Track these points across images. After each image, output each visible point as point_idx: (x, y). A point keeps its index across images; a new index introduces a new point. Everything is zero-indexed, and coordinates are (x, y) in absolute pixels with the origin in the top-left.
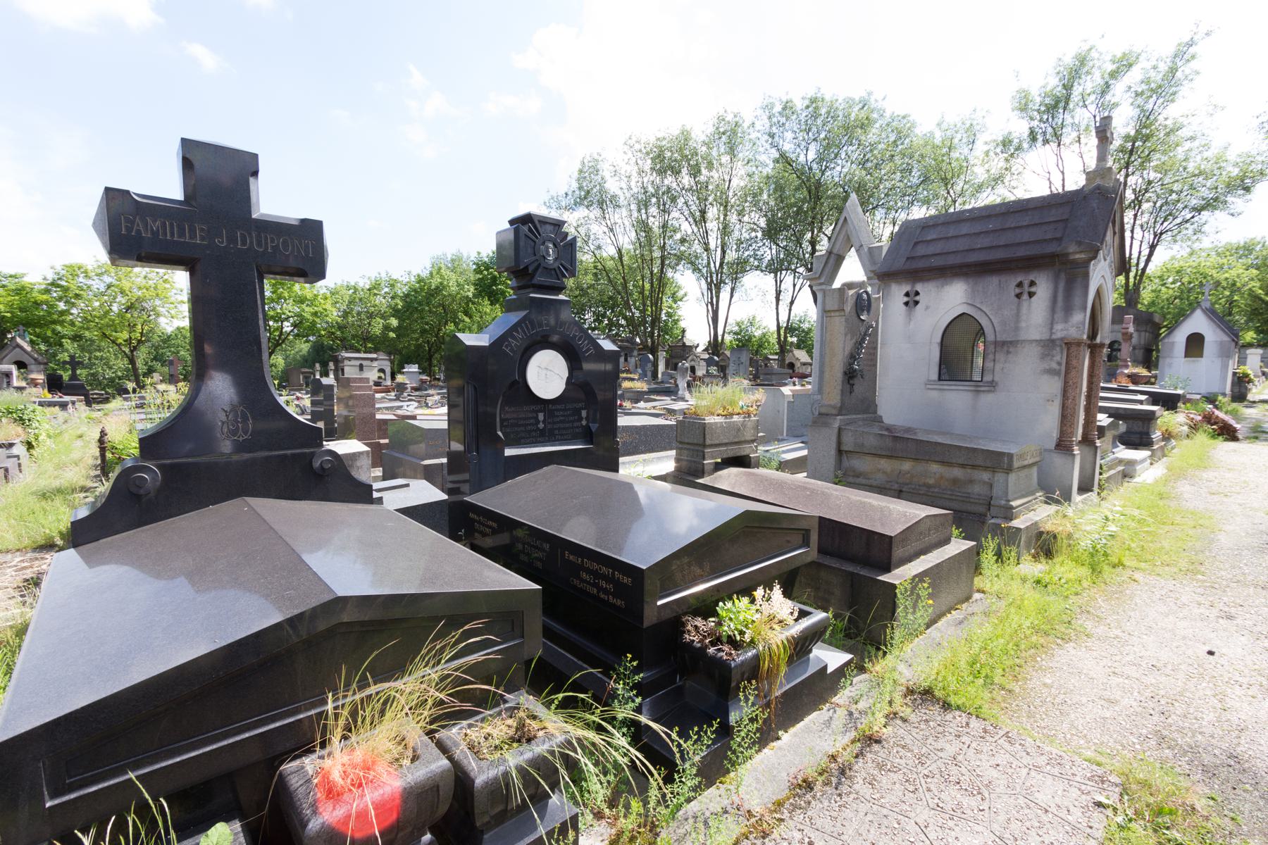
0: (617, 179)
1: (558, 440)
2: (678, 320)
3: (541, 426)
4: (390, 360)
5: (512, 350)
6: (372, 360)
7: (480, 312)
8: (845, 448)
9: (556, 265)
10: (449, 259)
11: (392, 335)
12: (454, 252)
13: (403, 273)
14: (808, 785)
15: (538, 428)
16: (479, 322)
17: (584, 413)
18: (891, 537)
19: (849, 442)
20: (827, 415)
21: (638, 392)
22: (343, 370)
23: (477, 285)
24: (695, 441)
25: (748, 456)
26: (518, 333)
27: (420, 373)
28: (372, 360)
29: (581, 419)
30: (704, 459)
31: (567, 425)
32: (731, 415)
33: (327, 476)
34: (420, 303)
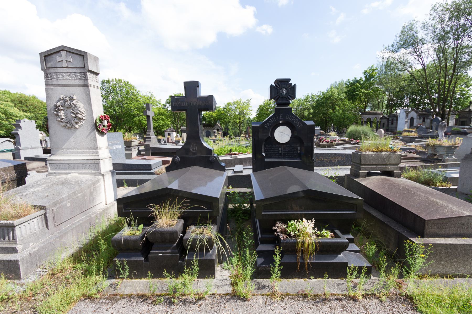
0: (425, 29)
1: (287, 157)
2: (468, 97)
3: (280, 152)
7: (344, 104)
10: (338, 84)
11: (311, 116)
12: (340, 80)
13: (318, 92)
14: (305, 296)
16: (343, 108)
18: (425, 220)
21: (411, 137)
23: (346, 93)
24: (357, 162)
25: (392, 171)
26: (270, 121)
27: (320, 130)
29: (298, 150)
30: (360, 170)
31: (291, 152)
32: (382, 151)
34: (322, 103)
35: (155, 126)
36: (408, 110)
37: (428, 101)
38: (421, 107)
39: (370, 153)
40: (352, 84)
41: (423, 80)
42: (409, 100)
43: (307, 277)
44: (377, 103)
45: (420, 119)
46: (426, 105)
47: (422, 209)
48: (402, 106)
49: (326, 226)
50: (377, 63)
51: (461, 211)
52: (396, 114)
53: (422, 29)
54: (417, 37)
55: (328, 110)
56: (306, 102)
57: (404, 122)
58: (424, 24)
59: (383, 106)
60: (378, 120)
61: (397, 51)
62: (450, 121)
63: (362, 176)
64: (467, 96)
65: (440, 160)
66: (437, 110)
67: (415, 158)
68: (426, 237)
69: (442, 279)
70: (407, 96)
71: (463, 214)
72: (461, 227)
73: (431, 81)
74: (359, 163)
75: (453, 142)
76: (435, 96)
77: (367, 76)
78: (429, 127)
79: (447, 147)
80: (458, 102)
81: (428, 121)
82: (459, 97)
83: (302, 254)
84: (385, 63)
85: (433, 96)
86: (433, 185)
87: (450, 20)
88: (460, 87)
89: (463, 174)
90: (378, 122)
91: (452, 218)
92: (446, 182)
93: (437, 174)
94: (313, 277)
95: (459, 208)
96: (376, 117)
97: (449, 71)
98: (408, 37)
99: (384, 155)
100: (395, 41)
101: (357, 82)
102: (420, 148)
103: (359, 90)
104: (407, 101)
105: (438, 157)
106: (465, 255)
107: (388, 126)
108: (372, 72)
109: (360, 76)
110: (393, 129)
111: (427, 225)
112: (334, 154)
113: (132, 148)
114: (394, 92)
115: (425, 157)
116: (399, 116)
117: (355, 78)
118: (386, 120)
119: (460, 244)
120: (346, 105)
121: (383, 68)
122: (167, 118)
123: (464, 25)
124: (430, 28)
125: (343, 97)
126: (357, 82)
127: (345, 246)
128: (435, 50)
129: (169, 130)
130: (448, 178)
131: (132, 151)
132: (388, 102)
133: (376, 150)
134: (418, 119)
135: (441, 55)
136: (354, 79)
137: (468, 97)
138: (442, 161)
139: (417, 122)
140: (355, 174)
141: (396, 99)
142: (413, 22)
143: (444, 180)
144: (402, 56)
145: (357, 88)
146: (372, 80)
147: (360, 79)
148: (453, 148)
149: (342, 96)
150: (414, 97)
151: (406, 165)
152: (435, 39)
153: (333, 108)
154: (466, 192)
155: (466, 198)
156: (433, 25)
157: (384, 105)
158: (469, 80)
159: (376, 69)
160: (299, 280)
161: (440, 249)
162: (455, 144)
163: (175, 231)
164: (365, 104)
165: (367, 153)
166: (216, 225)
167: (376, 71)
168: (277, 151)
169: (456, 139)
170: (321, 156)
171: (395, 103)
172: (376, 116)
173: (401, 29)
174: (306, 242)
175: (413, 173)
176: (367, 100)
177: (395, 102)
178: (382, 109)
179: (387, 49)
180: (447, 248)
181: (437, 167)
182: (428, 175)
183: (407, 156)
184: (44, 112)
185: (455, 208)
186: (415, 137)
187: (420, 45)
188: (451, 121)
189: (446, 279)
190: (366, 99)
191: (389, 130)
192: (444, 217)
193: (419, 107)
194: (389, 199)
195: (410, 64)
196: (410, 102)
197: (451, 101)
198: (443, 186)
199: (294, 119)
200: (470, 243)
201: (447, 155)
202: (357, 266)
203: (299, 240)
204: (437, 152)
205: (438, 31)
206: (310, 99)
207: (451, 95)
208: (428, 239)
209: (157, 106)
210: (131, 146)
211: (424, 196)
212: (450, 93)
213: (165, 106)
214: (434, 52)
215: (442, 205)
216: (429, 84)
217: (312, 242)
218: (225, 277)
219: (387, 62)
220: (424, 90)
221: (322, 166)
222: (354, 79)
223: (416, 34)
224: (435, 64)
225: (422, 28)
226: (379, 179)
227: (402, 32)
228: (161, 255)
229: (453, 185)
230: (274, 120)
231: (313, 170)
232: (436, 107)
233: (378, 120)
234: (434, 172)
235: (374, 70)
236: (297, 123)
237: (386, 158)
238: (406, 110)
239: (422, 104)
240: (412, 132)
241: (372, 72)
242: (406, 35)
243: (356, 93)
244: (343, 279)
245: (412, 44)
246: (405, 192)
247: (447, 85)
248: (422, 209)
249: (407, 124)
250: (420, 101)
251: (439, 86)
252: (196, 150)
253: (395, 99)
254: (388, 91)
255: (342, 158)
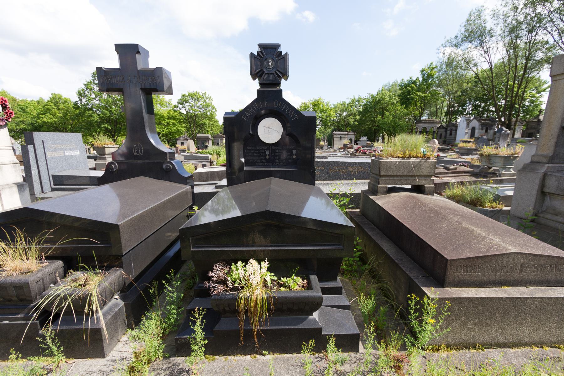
0: (495, 18)
2: (539, 105)
3: (267, 157)
4: (355, 135)
5: (247, 118)
6: (345, 135)
8: (547, 190)
9: (273, 71)
10: (391, 85)
11: (357, 123)
12: (393, 81)
15: (266, 158)
17: (294, 152)
18: (447, 260)
19: (552, 185)
20: (538, 163)
21: (468, 149)
22: (334, 139)
27: (367, 140)
28: (345, 135)
30: (379, 184)
32: (410, 157)
33: (169, 171)
35: (164, 133)
36: (469, 118)
37: (494, 109)
38: (485, 115)
39: (394, 159)
40: (406, 86)
41: (489, 83)
42: (472, 107)
43: (257, 351)
44: (435, 110)
45: (482, 129)
46: (491, 113)
47: (449, 241)
48: (463, 114)
49: (297, 269)
50: (437, 59)
51: (503, 245)
52: (456, 123)
53: (492, 18)
54: (485, 27)
55: (377, 116)
56: (351, 106)
57: (464, 133)
58: (494, 11)
59: (442, 114)
60: (435, 129)
61: (460, 45)
62: (516, 133)
63: (381, 193)
64: (537, 103)
65: (495, 174)
66: (503, 119)
67: (465, 172)
68: (448, 287)
69: (467, 351)
70: (470, 102)
71: (506, 251)
72: (502, 270)
73: (498, 84)
74: (377, 173)
75: (512, 150)
76: (502, 103)
77: (424, 75)
78: (492, 139)
79: (505, 157)
80: (527, 111)
81: (491, 132)
82: (529, 104)
83: (247, 316)
84: (446, 60)
85: (500, 102)
86: (480, 205)
87: (525, 8)
88: (530, 93)
89: (519, 190)
90: (434, 132)
91: (488, 256)
92: (498, 202)
93: (487, 191)
94: (267, 353)
95: (502, 239)
96: (433, 126)
97: (519, 72)
98: (474, 27)
99: (412, 162)
100: (459, 32)
101: (412, 83)
102: (476, 161)
103: (415, 93)
104: (469, 108)
105: (493, 171)
106: (504, 314)
107: (445, 137)
108: (431, 71)
109: (417, 75)
110: (451, 141)
111: (449, 268)
112: (354, 163)
113: (106, 157)
114: (455, 96)
115: (478, 170)
116: (458, 125)
117: (411, 78)
118: (444, 130)
119: (496, 298)
120: (397, 110)
121: (444, 66)
122: (180, 123)
123: (539, 13)
124: (502, 17)
125: (395, 101)
126: (412, 83)
127: (318, 303)
128: (505, 45)
129: (181, 139)
130: (500, 196)
131: (106, 160)
132: (447, 109)
133: (402, 155)
134: (480, 129)
135: (512, 51)
136: (409, 79)
137: (539, 105)
138: (497, 175)
139: (478, 133)
140: (373, 190)
141: (458, 105)
142: (481, 8)
143: (496, 199)
144: (466, 52)
145: (412, 90)
146: (430, 80)
147: (416, 79)
148: (512, 158)
149: (395, 99)
150: (478, 104)
151: (452, 180)
152: (506, 31)
153: (383, 115)
154: (521, 216)
155: (520, 223)
156: (504, 13)
157: (443, 112)
158: (541, 84)
159: (435, 67)
160: (244, 357)
161: (466, 306)
162: (515, 154)
163: (24, 283)
164: (421, 111)
165: (389, 159)
166: (123, 268)
167: (435, 70)
168: (262, 156)
169: (517, 147)
170: (336, 166)
171: (455, 110)
172: (433, 125)
173: (466, 17)
174: (253, 299)
175: (457, 191)
176: (424, 106)
177: (456, 109)
178: (441, 117)
179: (449, 43)
180: (477, 304)
181: (488, 182)
182: (476, 192)
183: (456, 169)
184: (17, 112)
185: (497, 240)
186: (472, 148)
187: (488, 38)
188: (517, 132)
189: (473, 351)
190: (422, 105)
191: (447, 143)
192: (477, 255)
193: (482, 116)
194: (406, 225)
195: (475, 62)
196: (473, 109)
197: (519, 108)
198: (493, 208)
199: (286, 106)
200: (512, 296)
201: (504, 168)
202: (333, 333)
203: (241, 296)
204: (492, 163)
205: (509, 20)
206: (357, 103)
207: (520, 102)
208: (449, 289)
209: (167, 107)
210: (105, 154)
211: (457, 222)
212: (518, 98)
213: (177, 108)
214: (504, 47)
215: (479, 234)
216: (496, 88)
217: (263, 298)
218: (125, 355)
219: (448, 58)
220: (490, 95)
221: (338, 180)
222: (409, 79)
223: (484, 24)
224: (504, 62)
225: (492, 16)
226: (404, 196)
227: (468, 20)
228: (7, 322)
229: (506, 206)
230: (257, 109)
231: (314, 184)
232: (501, 117)
233: (435, 129)
234: (483, 188)
235: (433, 68)
236: (291, 112)
237: (414, 167)
238: (467, 118)
239: (487, 112)
240: (469, 142)
241: (431, 71)
242: (473, 24)
243: (411, 96)
244: (314, 355)
245: (479, 37)
246: (432, 215)
247: (515, 89)
248: (449, 241)
249: (467, 135)
250: (484, 108)
251: (507, 89)
252: (141, 153)
253: (456, 105)
254: (448, 95)
255: (363, 169)
